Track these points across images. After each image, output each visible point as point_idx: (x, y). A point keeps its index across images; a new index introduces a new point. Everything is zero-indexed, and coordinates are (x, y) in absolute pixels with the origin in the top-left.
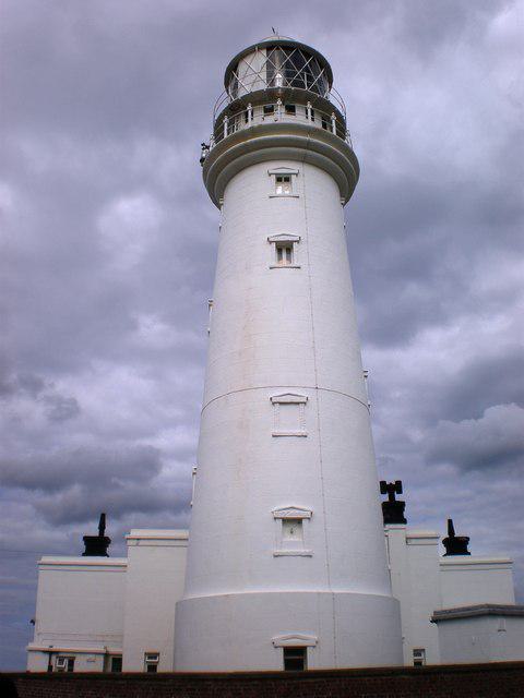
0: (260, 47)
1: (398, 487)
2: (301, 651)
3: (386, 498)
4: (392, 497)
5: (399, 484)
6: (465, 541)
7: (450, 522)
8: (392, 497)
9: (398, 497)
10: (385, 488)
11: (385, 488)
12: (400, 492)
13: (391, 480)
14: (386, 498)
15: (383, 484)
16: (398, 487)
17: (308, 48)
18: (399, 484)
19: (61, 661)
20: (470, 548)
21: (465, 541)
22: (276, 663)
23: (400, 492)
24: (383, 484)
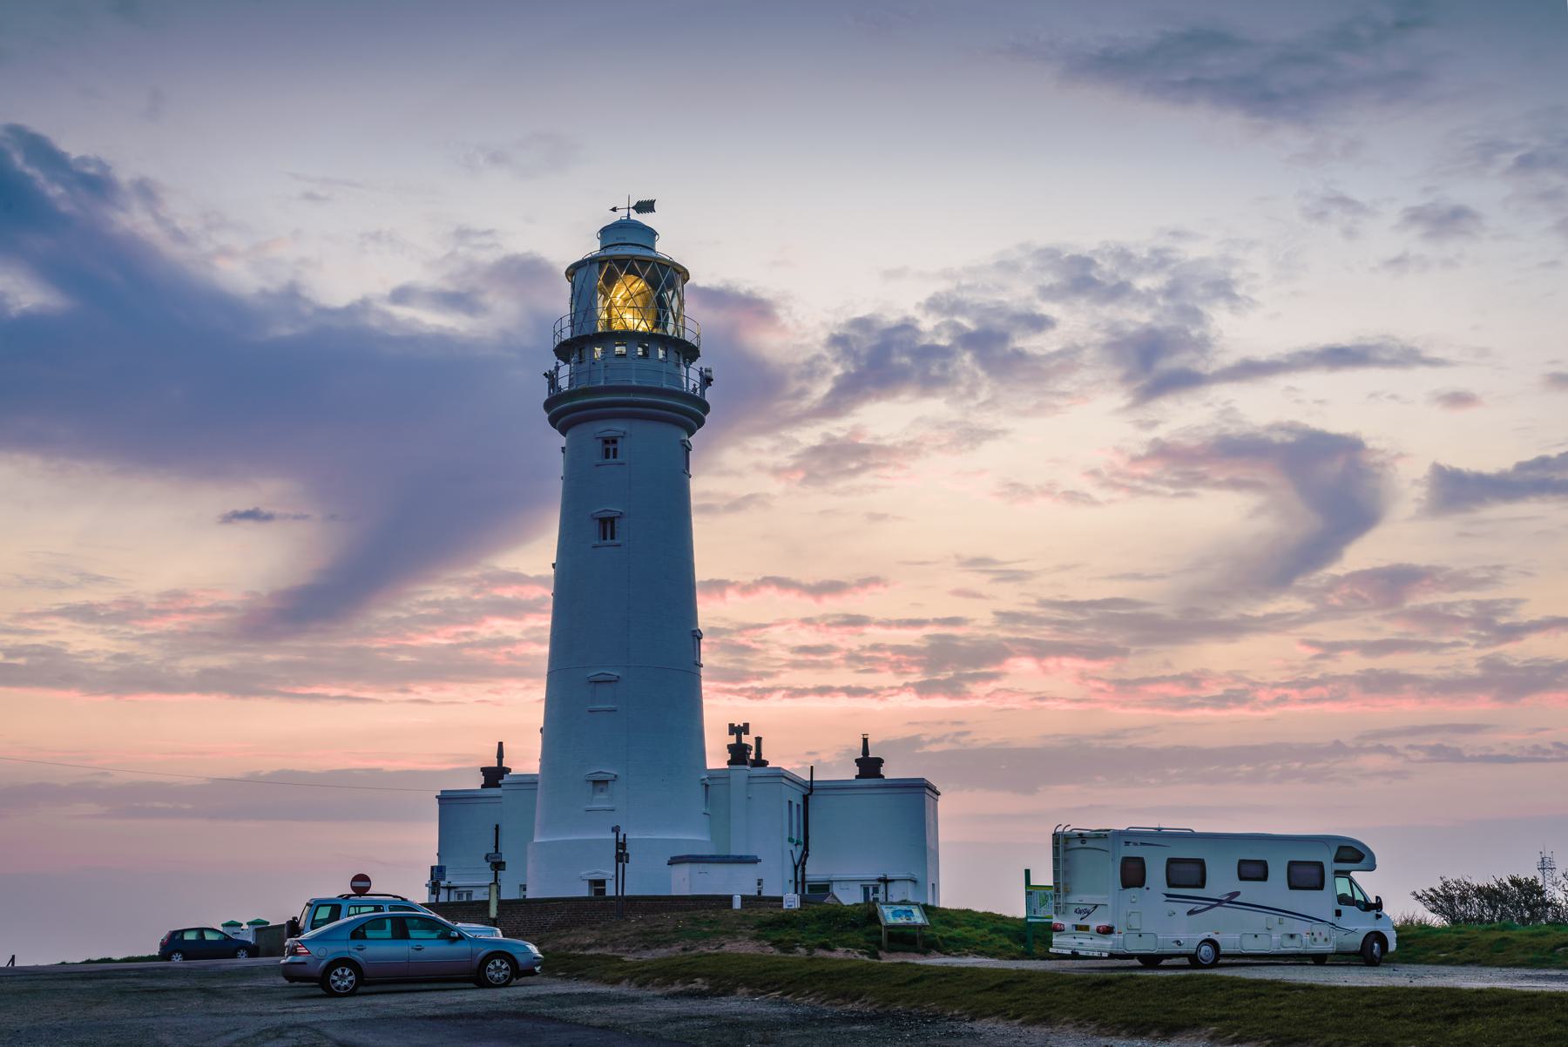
3: (733, 740)
4: (739, 739)
5: (746, 725)
6: (879, 762)
7: (501, 744)
8: (739, 739)
10: (733, 729)
11: (733, 729)
12: (747, 733)
13: (739, 723)
15: (731, 726)
16: (745, 729)
18: (746, 725)
19: (460, 895)
20: (883, 771)
21: (879, 762)
22: (584, 891)
23: (747, 733)
24: (731, 726)
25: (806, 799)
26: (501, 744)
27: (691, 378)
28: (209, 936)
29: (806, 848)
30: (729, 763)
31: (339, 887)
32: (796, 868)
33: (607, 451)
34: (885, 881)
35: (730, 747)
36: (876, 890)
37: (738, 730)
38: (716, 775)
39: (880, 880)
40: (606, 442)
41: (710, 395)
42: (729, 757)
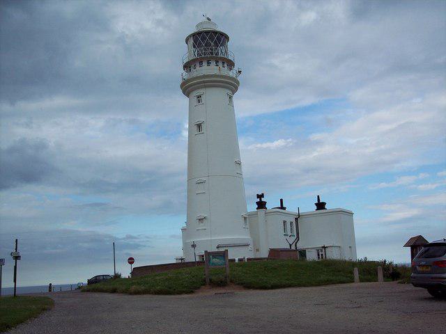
0: (190, 36)
1: (262, 196)
3: (258, 200)
4: (261, 200)
5: (263, 194)
7: (318, 196)
8: (261, 200)
9: (263, 199)
14: (258, 200)
16: (262, 196)
18: (263, 194)
26: (318, 196)
34: (324, 247)
36: (322, 251)
42: (257, 206)
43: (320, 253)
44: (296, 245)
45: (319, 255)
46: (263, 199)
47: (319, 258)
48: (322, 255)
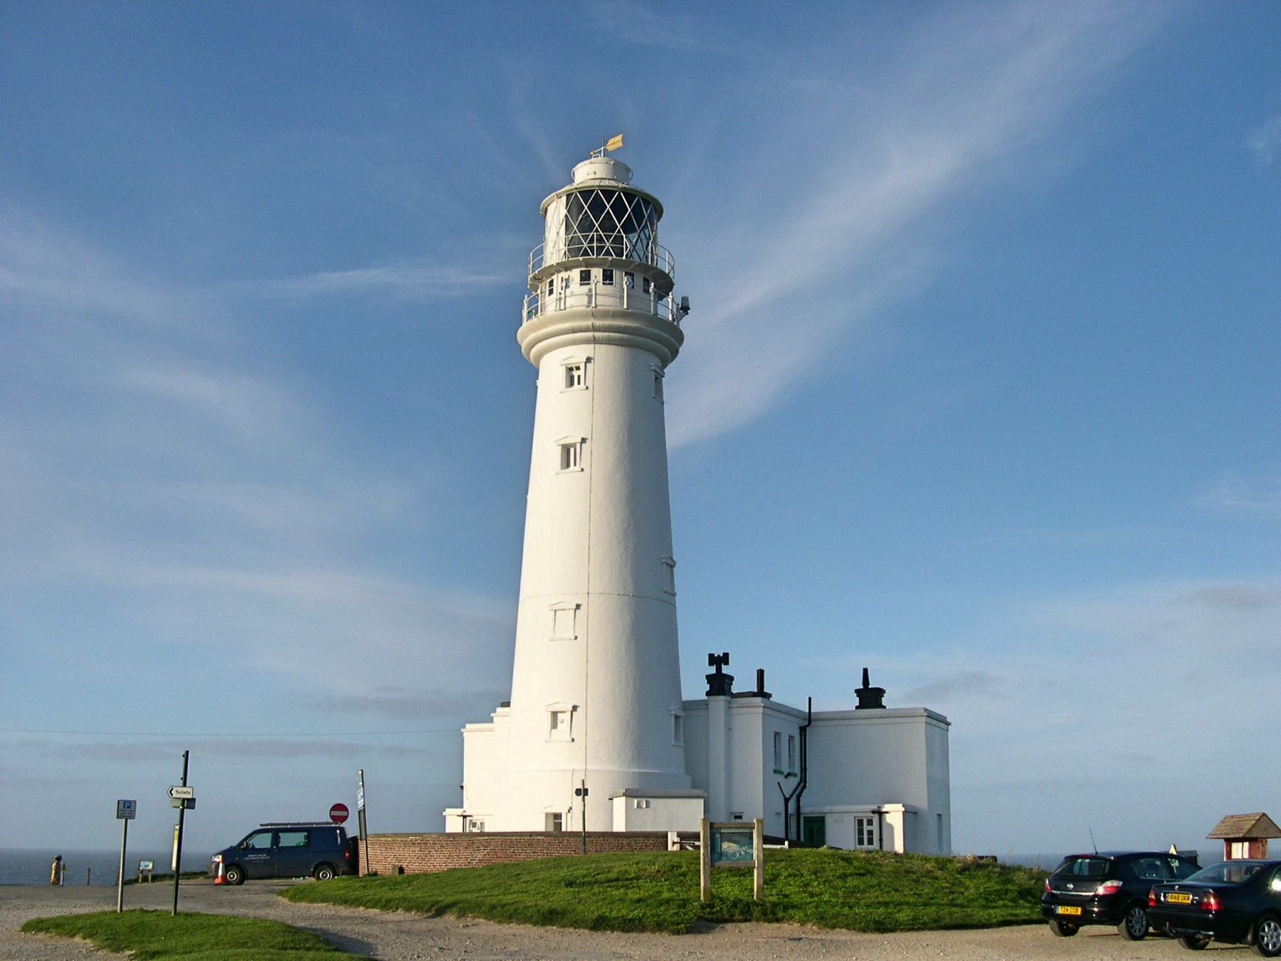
1: (725, 659)
2: (557, 816)
3: (713, 670)
4: (719, 669)
5: (726, 655)
6: (880, 692)
7: (865, 671)
8: (719, 669)
9: (725, 670)
10: (713, 660)
11: (713, 660)
12: (727, 663)
13: (719, 652)
14: (713, 670)
15: (711, 656)
16: (725, 659)
17: (647, 195)
18: (726, 655)
20: (884, 701)
21: (880, 692)
22: (539, 825)
23: (727, 663)
24: (711, 656)
25: (803, 730)
26: (865, 671)
27: (667, 309)
28: (288, 840)
29: (803, 781)
30: (708, 694)
31: (322, 816)
32: (787, 801)
33: (572, 377)
35: (709, 678)
36: (870, 822)
37: (718, 660)
38: (689, 706)
39: (874, 812)
40: (571, 369)
41: (685, 325)
42: (707, 687)
43: (866, 828)
44: (798, 801)
45: (861, 832)
46: (725, 670)
47: (861, 842)
48: (870, 833)
